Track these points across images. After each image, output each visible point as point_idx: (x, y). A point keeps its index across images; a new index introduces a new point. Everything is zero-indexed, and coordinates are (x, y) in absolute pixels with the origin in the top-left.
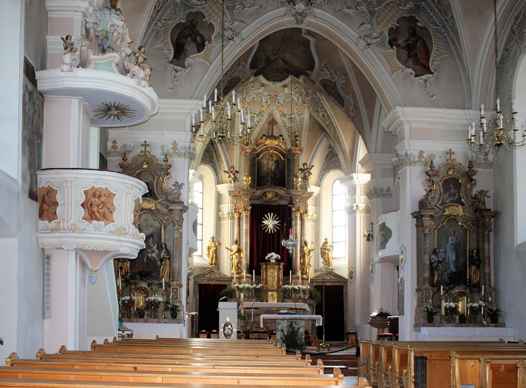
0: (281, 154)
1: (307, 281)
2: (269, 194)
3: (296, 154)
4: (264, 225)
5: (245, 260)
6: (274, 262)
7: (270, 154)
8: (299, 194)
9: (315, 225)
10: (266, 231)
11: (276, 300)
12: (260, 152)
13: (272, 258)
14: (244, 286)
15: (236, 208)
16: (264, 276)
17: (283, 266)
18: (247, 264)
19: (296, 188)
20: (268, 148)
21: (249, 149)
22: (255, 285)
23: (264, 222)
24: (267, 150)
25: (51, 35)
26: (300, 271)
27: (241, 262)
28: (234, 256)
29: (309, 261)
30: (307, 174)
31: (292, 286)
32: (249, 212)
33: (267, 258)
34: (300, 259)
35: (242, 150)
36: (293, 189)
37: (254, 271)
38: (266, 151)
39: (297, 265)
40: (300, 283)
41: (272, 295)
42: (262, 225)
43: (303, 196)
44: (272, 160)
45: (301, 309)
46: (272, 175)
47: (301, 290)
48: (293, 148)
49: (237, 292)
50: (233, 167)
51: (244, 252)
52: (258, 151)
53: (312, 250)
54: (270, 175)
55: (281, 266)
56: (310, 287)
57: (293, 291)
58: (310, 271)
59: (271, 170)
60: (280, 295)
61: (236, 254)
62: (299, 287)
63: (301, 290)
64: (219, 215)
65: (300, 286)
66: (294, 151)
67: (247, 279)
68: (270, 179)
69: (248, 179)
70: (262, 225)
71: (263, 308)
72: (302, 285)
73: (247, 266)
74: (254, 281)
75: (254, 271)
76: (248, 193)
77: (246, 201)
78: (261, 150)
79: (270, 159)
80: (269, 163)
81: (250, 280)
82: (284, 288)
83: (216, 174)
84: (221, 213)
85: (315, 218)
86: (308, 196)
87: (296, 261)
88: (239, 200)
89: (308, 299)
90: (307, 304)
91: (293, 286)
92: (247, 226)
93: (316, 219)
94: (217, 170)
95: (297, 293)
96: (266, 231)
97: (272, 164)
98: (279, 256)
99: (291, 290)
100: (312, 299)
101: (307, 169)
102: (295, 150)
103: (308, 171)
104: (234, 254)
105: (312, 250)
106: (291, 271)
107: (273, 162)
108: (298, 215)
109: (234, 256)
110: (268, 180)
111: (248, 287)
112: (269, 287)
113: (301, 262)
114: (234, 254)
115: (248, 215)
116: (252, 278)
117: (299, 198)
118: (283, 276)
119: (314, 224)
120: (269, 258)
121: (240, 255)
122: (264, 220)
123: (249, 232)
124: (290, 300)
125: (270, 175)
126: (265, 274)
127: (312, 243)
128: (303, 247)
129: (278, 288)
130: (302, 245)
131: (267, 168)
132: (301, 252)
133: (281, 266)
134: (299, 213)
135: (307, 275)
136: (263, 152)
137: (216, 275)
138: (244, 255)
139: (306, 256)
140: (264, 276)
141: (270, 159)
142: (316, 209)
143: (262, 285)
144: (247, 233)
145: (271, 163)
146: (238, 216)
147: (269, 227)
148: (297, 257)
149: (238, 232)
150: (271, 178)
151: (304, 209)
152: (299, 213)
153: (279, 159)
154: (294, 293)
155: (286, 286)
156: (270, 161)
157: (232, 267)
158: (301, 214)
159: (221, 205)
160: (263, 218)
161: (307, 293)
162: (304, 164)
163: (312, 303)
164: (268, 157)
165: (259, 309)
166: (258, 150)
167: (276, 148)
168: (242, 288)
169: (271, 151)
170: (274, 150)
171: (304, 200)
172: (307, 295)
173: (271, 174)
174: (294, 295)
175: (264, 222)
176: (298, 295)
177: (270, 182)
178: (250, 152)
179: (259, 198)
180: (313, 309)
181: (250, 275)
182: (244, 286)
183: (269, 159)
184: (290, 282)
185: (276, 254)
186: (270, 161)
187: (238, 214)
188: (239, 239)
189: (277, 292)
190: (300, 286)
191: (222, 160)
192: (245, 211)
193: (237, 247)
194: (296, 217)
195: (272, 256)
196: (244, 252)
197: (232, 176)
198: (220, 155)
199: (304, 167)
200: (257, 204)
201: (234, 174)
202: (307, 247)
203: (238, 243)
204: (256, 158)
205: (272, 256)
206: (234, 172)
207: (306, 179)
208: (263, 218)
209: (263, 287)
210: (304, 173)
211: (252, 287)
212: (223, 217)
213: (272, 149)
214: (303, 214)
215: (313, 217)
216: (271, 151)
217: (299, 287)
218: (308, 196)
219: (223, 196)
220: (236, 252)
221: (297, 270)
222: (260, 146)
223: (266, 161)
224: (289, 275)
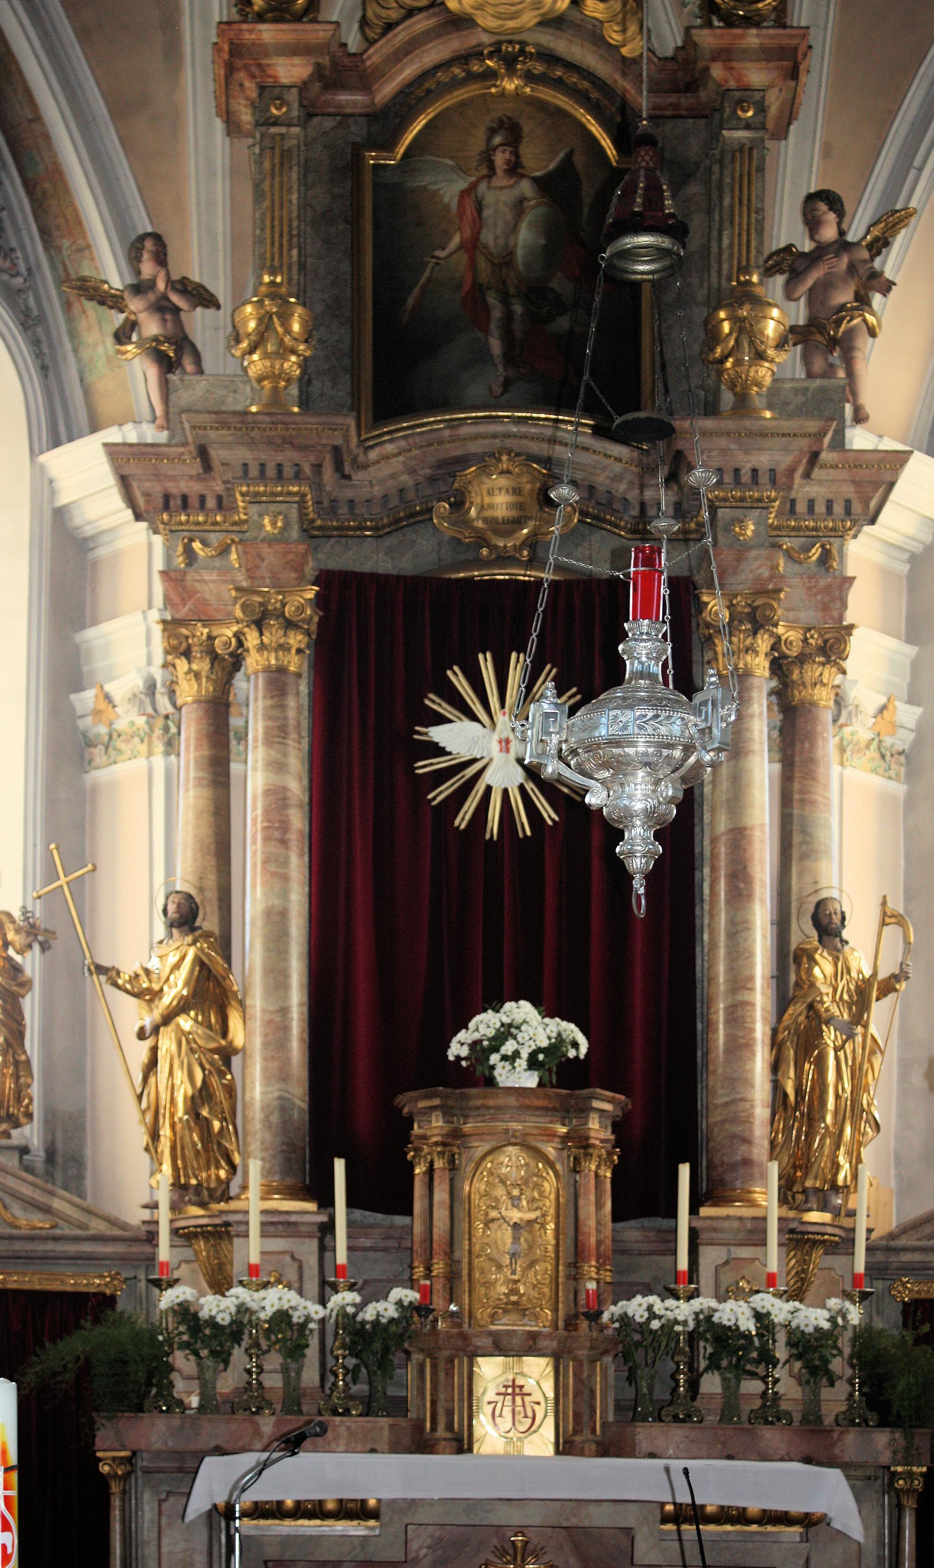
0: (583, 98)
1: (838, 1262)
2: (485, 470)
3: (740, 103)
4: (440, 763)
5: (267, 1078)
6: (531, 1080)
7: (501, 110)
8: (763, 459)
9: (910, 802)
10: (463, 819)
11: (548, 1431)
12: (405, 92)
13: (509, 1047)
14: (242, 1309)
15: (183, 612)
16: (441, 1215)
17: (618, 1126)
18: (284, 1106)
19: (742, 402)
20: (477, 54)
21: (293, 50)
22: (345, 1298)
23: (437, 734)
24: (471, 77)
25: (112, 679)
26: (774, 1169)
27: (230, 1090)
28: (167, 1043)
29: (858, 1086)
30: (844, 296)
31: (697, 1304)
32: (296, 639)
33: (458, 1048)
34: (776, 1067)
35: (230, 69)
36: (711, 409)
37: (339, 1166)
38: (455, 84)
39: (748, 1120)
40: (771, 1280)
41: (515, 1390)
42: (425, 767)
43: (803, 490)
44: (515, 169)
45: (783, 1518)
46: (518, 309)
47: (781, 1337)
48: (707, 39)
49: (181, 1360)
50: (157, 238)
51: (257, 1001)
52: (387, 90)
53: (887, 988)
54: (497, 313)
55: (594, 1124)
56: (868, 1315)
57: (705, 1348)
58: (866, 1172)
59: (507, 259)
60: (584, 1392)
61: (185, 1022)
62: (759, 1316)
63: (781, 1337)
64: (73, 715)
65: (766, 1301)
66: (717, 71)
67: (278, 1244)
68: (496, 346)
69: (285, 319)
70: (425, 767)
71: (413, 1503)
72: (797, 1293)
73: (285, 1122)
74: (342, 1257)
75: (339, 1166)
76: (288, 456)
77: (271, 541)
78: (408, 71)
79: (500, 159)
80: (490, 198)
81: (309, 1249)
82: (625, 1319)
83: (38, 355)
84: (87, 698)
85: (903, 740)
86: (848, 491)
87: (741, 1081)
88: (214, 538)
89: (848, 1420)
90: (836, 1475)
91: (704, 1302)
92: (278, 766)
93: (918, 743)
94: (41, 319)
95: (740, 1371)
96: (463, 819)
97: (519, 206)
98: (571, 1030)
99: (692, 1337)
100: (883, 1423)
101: (842, 245)
102: (725, 55)
103: (852, 268)
104: (167, 1019)
105: (887, 988)
106: (684, 1171)
107: (526, 187)
108: (760, 665)
109: (167, 1043)
110: (482, 356)
111: (282, 1317)
112: (482, 1314)
113: (777, 1088)
114: (167, 1019)
115: (294, 663)
116: (328, 1228)
117: (761, 504)
118: (617, 1216)
119: (899, 789)
120: (480, 1051)
121: (224, 1032)
122: (441, 720)
123: (298, 821)
124: (677, 1433)
125: (497, 313)
126: (441, 1195)
127: (887, 917)
128: (804, 957)
129: (571, 1324)
130: (795, 940)
131: (472, 245)
132: (783, 1002)
133: (594, 1124)
134: (763, 643)
135: (836, 1212)
136: (430, 96)
137: (17, 1210)
138: (257, 1025)
139: (830, 1036)
140: (441, 1215)
141: (500, 159)
142: (916, 665)
143: (411, 1296)
144: (284, 826)
145: (507, 196)
146: (207, 687)
147: (488, 778)
148: (749, 1045)
149: (206, 831)
150: (508, 337)
151: (809, 616)
152: (763, 643)
153: (579, 160)
154: (714, 1364)
155: (636, 1307)
156: (500, 180)
157: (155, 1136)
158: (779, 666)
159: (91, 633)
160: (435, 703)
161: (837, 1365)
162: (811, 198)
163: (885, 1457)
164: (477, 143)
165: (374, 1514)
166: (380, 73)
167: (549, 57)
168: (224, 1319)
169: (510, 85)
170: (529, 77)
171: (813, 536)
172: (841, 1390)
173: (505, 300)
174: (711, 1384)
175: (437, 734)
176: (752, 1387)
177: (497, 373)
178: (303, 87)
179: (397, 525)
180: (899, 1508)
181: (311, 1206)
182: (242, 1309)
183: (487, 158)
184: (683, 1263)
185: (549, 1010)
186: (500, 180)
187: (202, 665)
188: (212, 894)
189: (558, 1358)
190: (766, 1301)
191: (77, 223)
192: (259, 624)
193: (191, 953)
194: (744, 676)
195: (507, 1032)
196: (257, 1001)
197: (151, 327)
198: (57, 174)
199: (812, 224)
200: (374, 577)
201: (163, 308)
202: (836, 954)
203: (209, 921)
204: (372, 158)
205: (507, 1032)
206: (161, 285)
207: (833, 342)
208: (435, 703)
209: (422, 1309)
210: (810, 281)
211: (316, 1311)
212: (103, 730)
213: (510, 62)
214: (802, 659)
215: (895, 726)
216: (510, 85)
217: (759, 1316)
218: (848, 491)
219: (102, 552)
220: (182, 1007)
221: (747, 1162)
222: (400, 35)
223: (462, 184)
224: (672, 1213)
